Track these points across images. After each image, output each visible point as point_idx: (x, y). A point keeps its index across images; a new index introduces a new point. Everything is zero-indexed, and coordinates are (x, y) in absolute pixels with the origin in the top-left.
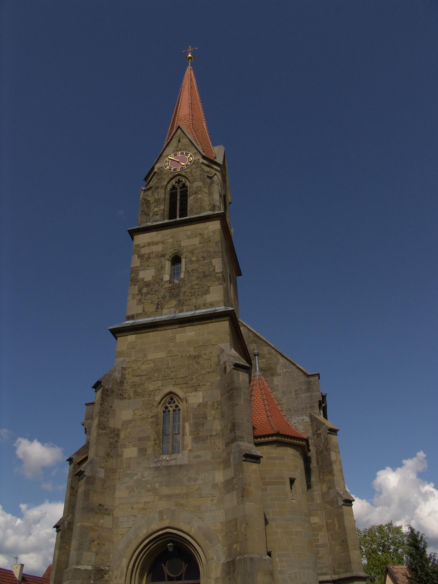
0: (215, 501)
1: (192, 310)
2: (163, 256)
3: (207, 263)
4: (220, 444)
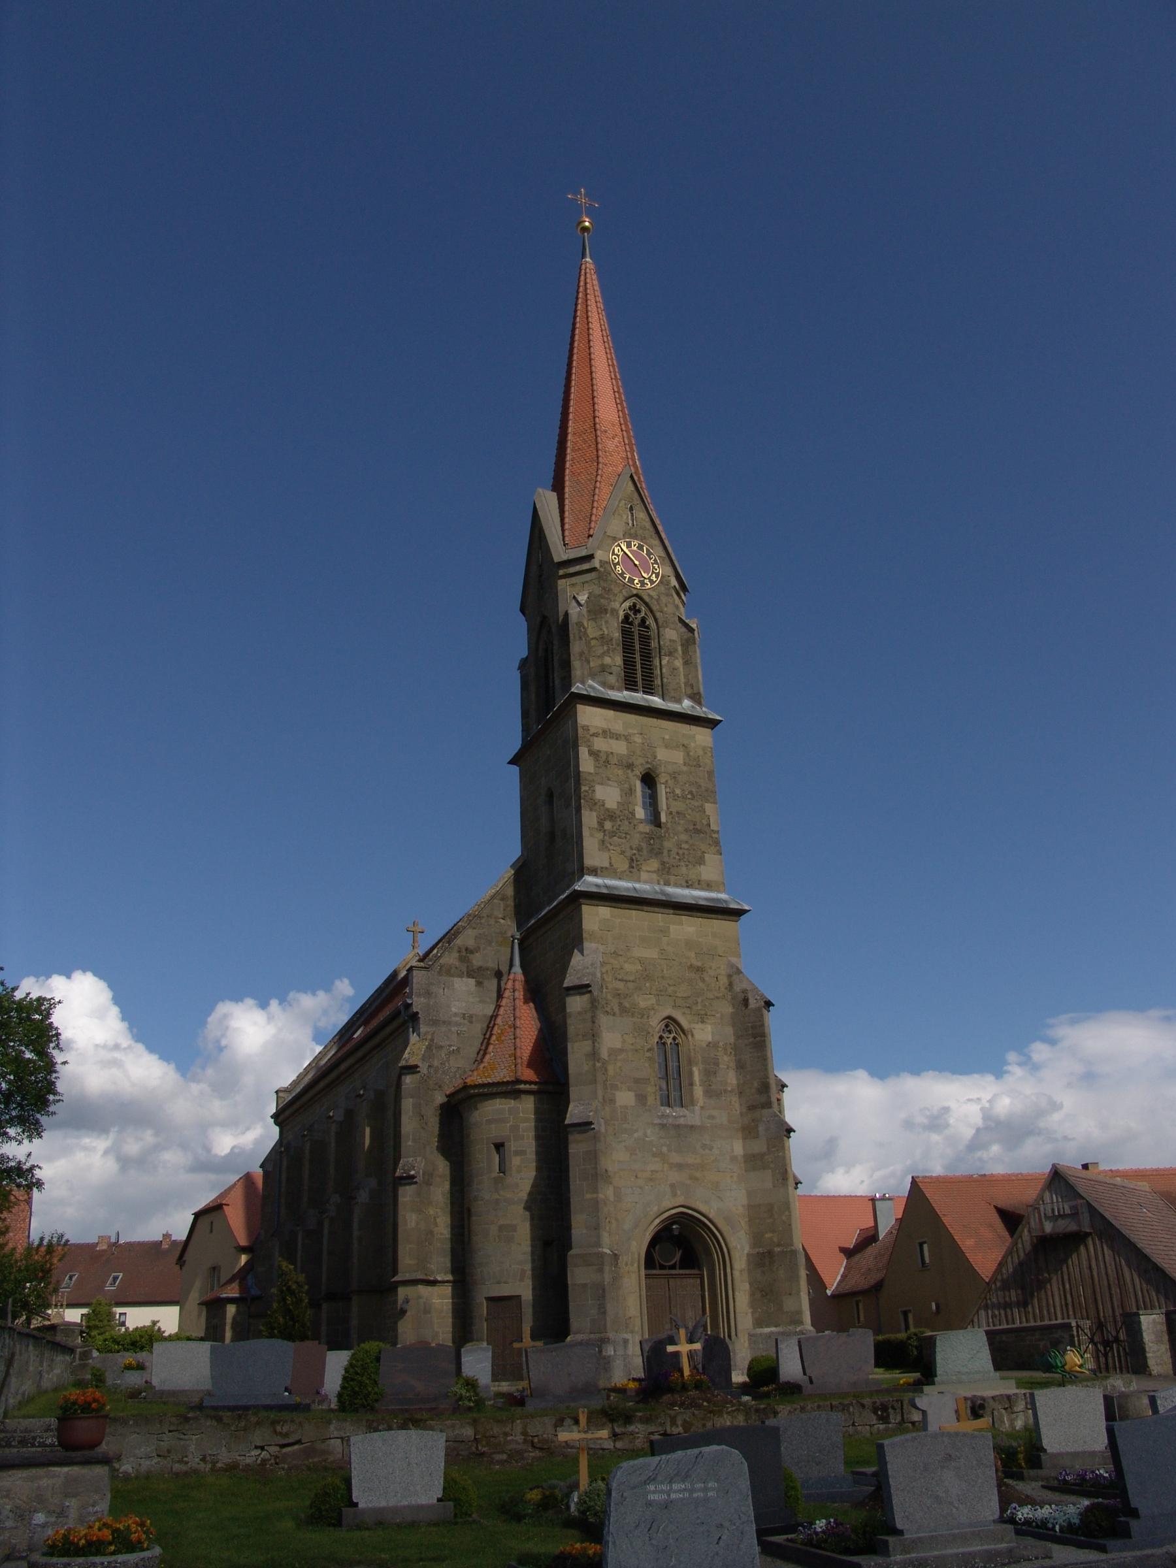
1: (681, 886)
2: (630, 766)
3: (698, 807)
4: (736, 1104)
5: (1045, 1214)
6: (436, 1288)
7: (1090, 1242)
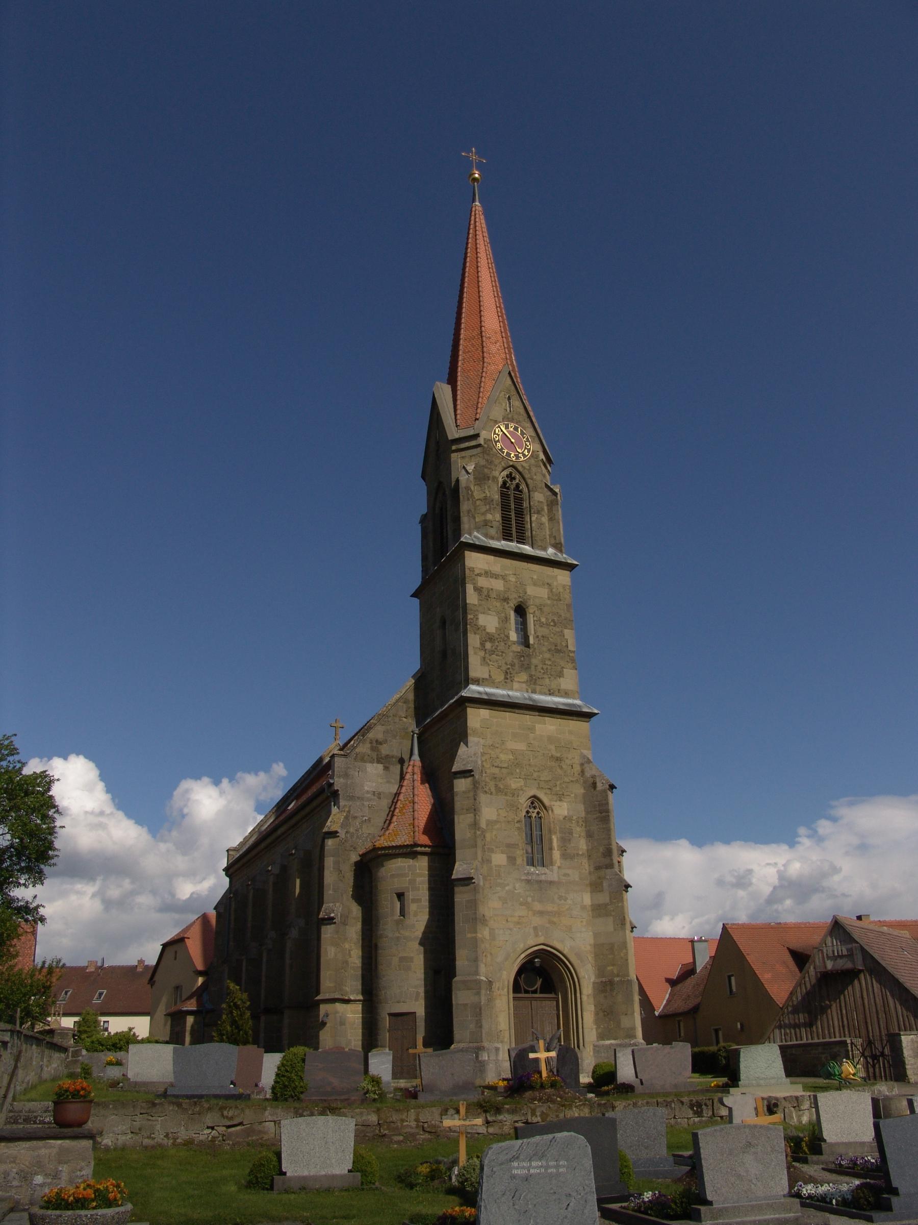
0: (584, 923)
1: (545, 694)
2: (506, 600)
4: (586, 866)
5: (827, 954)
6: (349, 1005)
7: (862, 976)
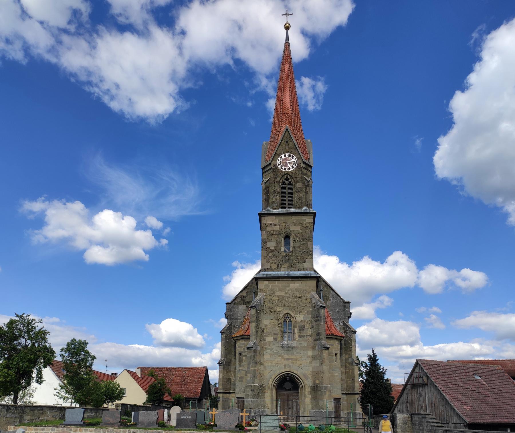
0: (308, 363)
4: (311, 340)
